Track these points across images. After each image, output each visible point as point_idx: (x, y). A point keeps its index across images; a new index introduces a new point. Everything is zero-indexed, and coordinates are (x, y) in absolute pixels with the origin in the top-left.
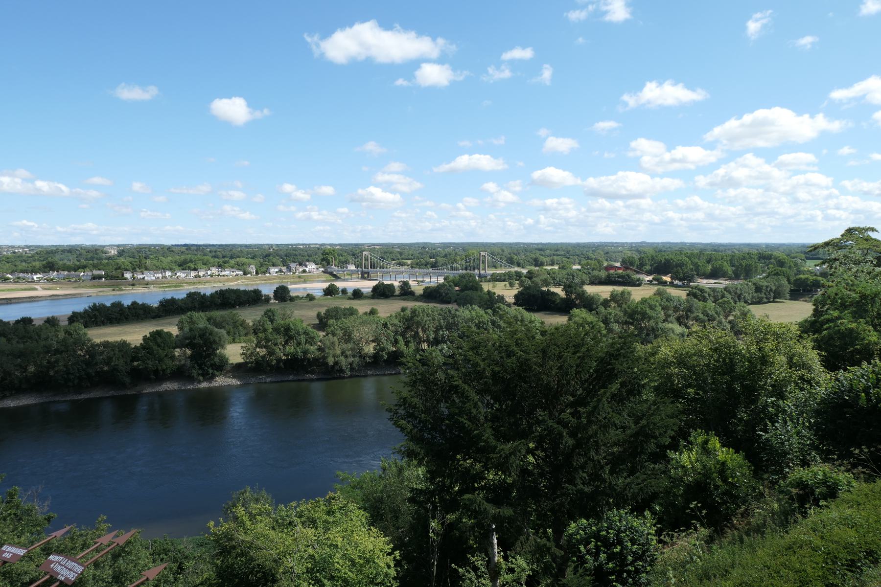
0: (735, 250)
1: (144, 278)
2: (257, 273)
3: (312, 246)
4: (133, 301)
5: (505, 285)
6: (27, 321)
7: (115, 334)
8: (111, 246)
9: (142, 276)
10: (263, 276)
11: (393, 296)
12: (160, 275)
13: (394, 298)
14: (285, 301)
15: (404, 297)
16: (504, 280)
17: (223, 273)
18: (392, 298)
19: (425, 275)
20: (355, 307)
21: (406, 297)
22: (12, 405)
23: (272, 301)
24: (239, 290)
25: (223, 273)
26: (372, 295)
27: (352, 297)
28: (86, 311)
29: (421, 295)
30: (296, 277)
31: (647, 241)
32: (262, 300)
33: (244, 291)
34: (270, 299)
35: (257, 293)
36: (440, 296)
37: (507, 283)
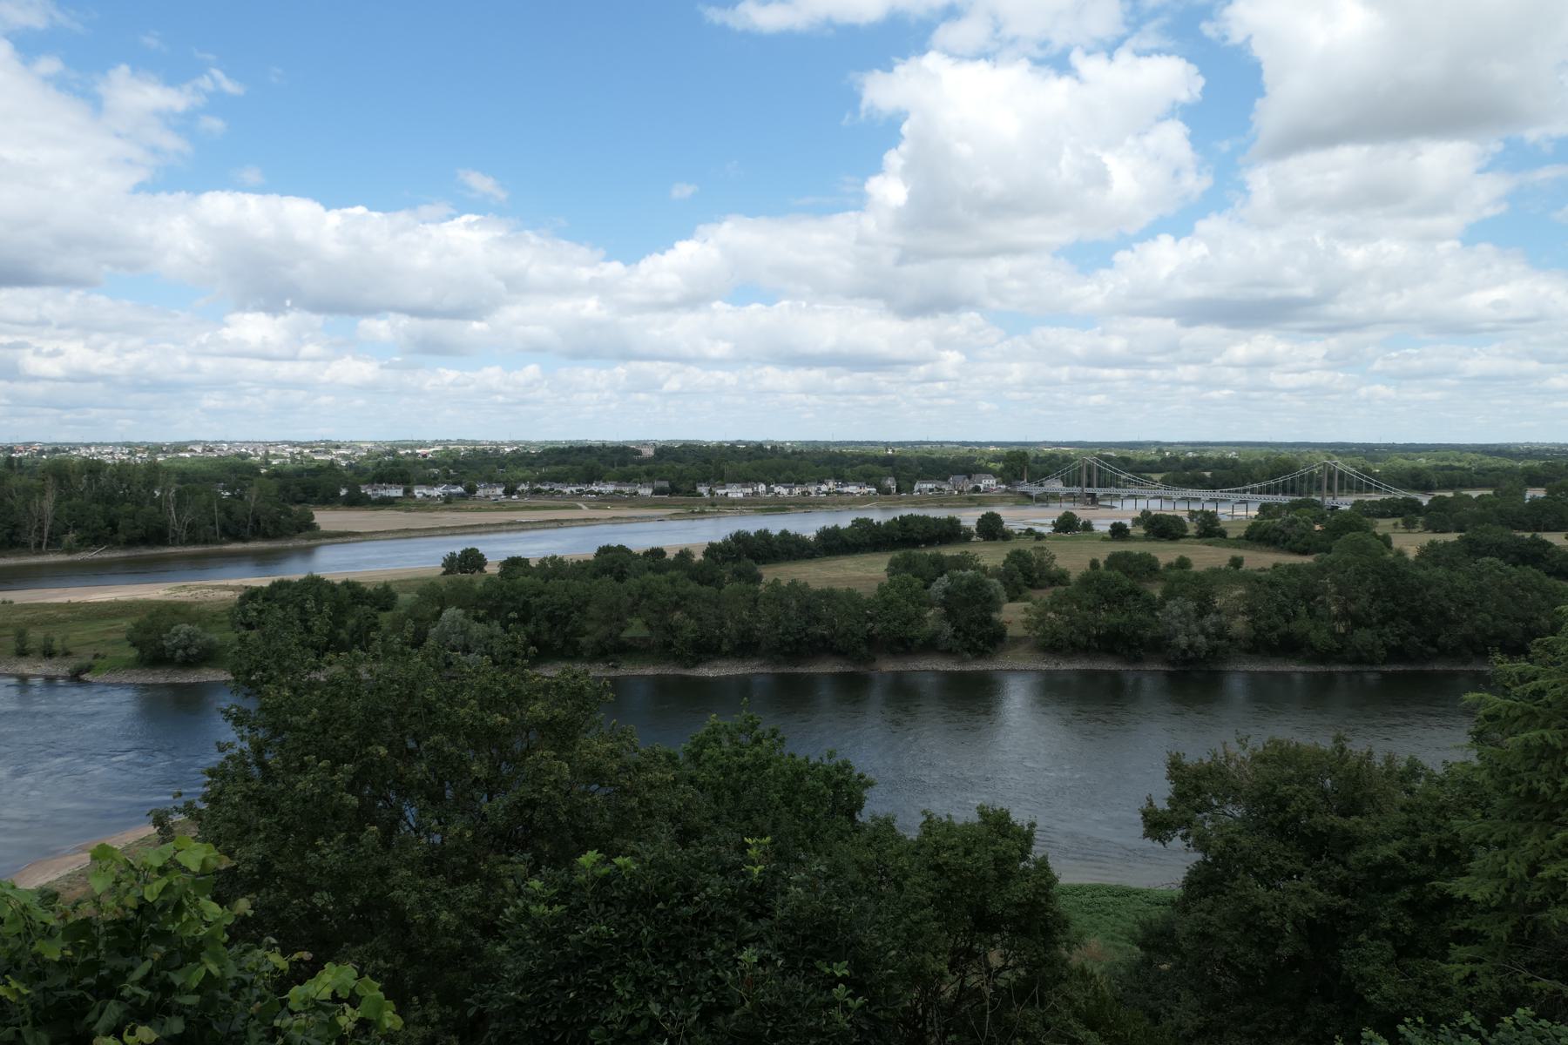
1: (726, 494)
3: (946, 446)
4: (782, 528)
6: (657, 553)
7: (56, 596)
8: (645, 444)
9: (723, 492)
12: (750, 491)
13: (1187, 540)
14: (995, 538)
15: (1208, 540)
16: (1393, 515)
17: (846, 489)
18: (1182, 540)
19: (1207, 501)
20: (1153, 554)
21: (1212, 539)
22: (711, 675)
23: (974, 539)
24: (928, 517)
25: (846, 489)
28: (725, 542)
29: (1239, 538)
30: (964, 498)
33: (935, 519)
36: (1285, 541)
37: (1399, 520)
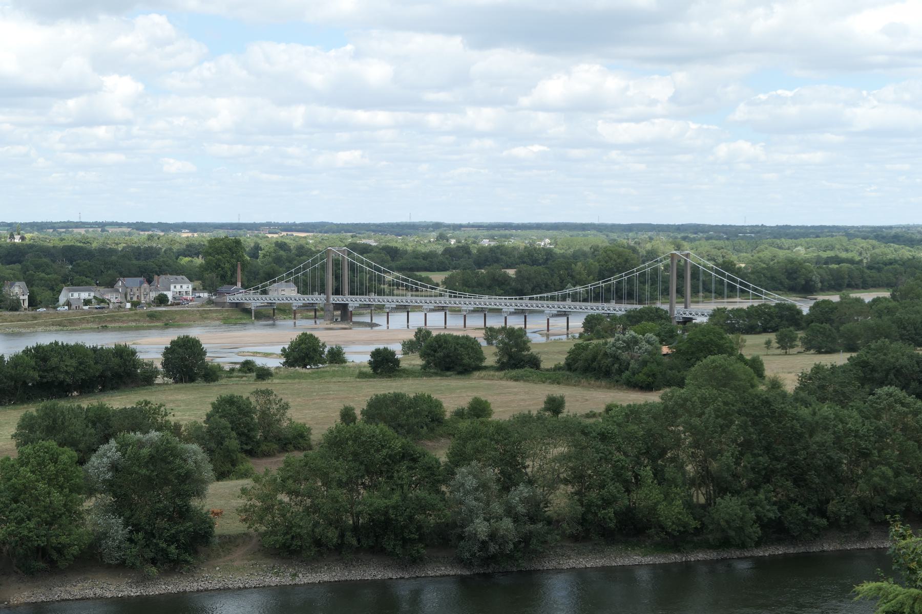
0: (879, 504)
2: (33, 303)
5: (768, 343)
10: (51, 311)
11: (479, 368)
13: (483, 373)
14: (192, 379)
15: (514, 373)
23: (159, 380)
26: (424, 367)
27: (369, 370)
29: (557, 368)
30: (142, 315)
31: (280, 222)
32: (136, 375)
33: (94, 350)
34: (155, 373)
35: (124, 355)
37: (772, 337)
